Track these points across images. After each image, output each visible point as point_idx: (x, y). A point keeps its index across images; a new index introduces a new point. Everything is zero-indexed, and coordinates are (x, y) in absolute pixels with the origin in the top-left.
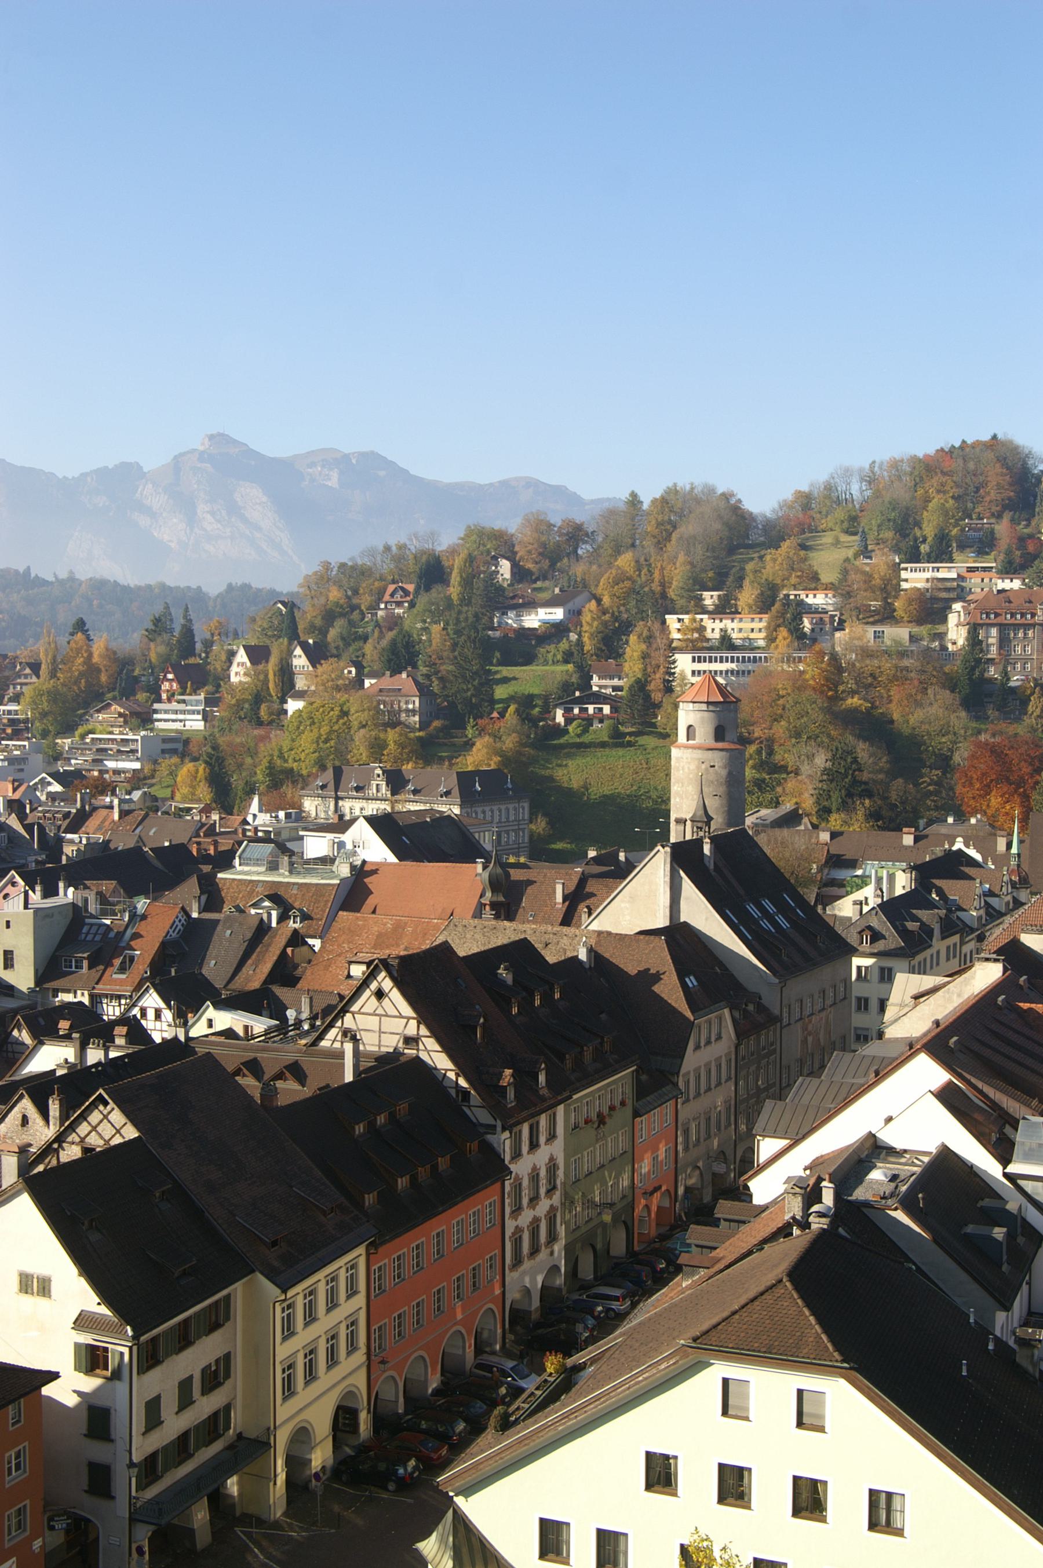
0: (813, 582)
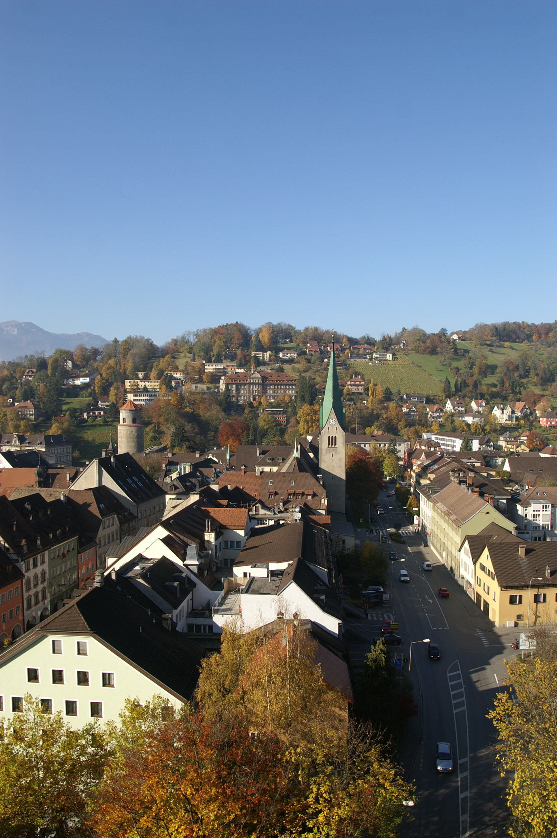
0: (176, 369)
